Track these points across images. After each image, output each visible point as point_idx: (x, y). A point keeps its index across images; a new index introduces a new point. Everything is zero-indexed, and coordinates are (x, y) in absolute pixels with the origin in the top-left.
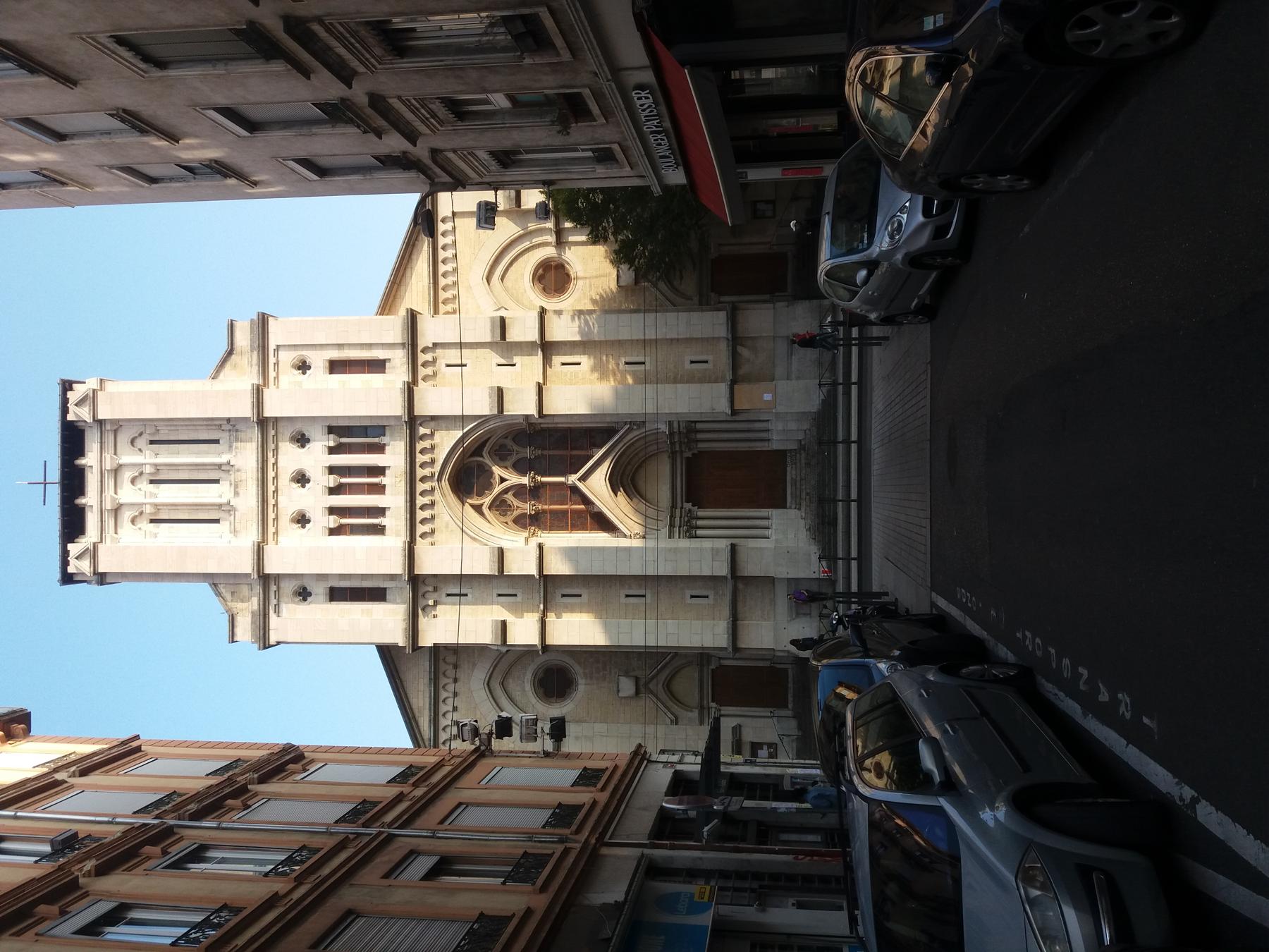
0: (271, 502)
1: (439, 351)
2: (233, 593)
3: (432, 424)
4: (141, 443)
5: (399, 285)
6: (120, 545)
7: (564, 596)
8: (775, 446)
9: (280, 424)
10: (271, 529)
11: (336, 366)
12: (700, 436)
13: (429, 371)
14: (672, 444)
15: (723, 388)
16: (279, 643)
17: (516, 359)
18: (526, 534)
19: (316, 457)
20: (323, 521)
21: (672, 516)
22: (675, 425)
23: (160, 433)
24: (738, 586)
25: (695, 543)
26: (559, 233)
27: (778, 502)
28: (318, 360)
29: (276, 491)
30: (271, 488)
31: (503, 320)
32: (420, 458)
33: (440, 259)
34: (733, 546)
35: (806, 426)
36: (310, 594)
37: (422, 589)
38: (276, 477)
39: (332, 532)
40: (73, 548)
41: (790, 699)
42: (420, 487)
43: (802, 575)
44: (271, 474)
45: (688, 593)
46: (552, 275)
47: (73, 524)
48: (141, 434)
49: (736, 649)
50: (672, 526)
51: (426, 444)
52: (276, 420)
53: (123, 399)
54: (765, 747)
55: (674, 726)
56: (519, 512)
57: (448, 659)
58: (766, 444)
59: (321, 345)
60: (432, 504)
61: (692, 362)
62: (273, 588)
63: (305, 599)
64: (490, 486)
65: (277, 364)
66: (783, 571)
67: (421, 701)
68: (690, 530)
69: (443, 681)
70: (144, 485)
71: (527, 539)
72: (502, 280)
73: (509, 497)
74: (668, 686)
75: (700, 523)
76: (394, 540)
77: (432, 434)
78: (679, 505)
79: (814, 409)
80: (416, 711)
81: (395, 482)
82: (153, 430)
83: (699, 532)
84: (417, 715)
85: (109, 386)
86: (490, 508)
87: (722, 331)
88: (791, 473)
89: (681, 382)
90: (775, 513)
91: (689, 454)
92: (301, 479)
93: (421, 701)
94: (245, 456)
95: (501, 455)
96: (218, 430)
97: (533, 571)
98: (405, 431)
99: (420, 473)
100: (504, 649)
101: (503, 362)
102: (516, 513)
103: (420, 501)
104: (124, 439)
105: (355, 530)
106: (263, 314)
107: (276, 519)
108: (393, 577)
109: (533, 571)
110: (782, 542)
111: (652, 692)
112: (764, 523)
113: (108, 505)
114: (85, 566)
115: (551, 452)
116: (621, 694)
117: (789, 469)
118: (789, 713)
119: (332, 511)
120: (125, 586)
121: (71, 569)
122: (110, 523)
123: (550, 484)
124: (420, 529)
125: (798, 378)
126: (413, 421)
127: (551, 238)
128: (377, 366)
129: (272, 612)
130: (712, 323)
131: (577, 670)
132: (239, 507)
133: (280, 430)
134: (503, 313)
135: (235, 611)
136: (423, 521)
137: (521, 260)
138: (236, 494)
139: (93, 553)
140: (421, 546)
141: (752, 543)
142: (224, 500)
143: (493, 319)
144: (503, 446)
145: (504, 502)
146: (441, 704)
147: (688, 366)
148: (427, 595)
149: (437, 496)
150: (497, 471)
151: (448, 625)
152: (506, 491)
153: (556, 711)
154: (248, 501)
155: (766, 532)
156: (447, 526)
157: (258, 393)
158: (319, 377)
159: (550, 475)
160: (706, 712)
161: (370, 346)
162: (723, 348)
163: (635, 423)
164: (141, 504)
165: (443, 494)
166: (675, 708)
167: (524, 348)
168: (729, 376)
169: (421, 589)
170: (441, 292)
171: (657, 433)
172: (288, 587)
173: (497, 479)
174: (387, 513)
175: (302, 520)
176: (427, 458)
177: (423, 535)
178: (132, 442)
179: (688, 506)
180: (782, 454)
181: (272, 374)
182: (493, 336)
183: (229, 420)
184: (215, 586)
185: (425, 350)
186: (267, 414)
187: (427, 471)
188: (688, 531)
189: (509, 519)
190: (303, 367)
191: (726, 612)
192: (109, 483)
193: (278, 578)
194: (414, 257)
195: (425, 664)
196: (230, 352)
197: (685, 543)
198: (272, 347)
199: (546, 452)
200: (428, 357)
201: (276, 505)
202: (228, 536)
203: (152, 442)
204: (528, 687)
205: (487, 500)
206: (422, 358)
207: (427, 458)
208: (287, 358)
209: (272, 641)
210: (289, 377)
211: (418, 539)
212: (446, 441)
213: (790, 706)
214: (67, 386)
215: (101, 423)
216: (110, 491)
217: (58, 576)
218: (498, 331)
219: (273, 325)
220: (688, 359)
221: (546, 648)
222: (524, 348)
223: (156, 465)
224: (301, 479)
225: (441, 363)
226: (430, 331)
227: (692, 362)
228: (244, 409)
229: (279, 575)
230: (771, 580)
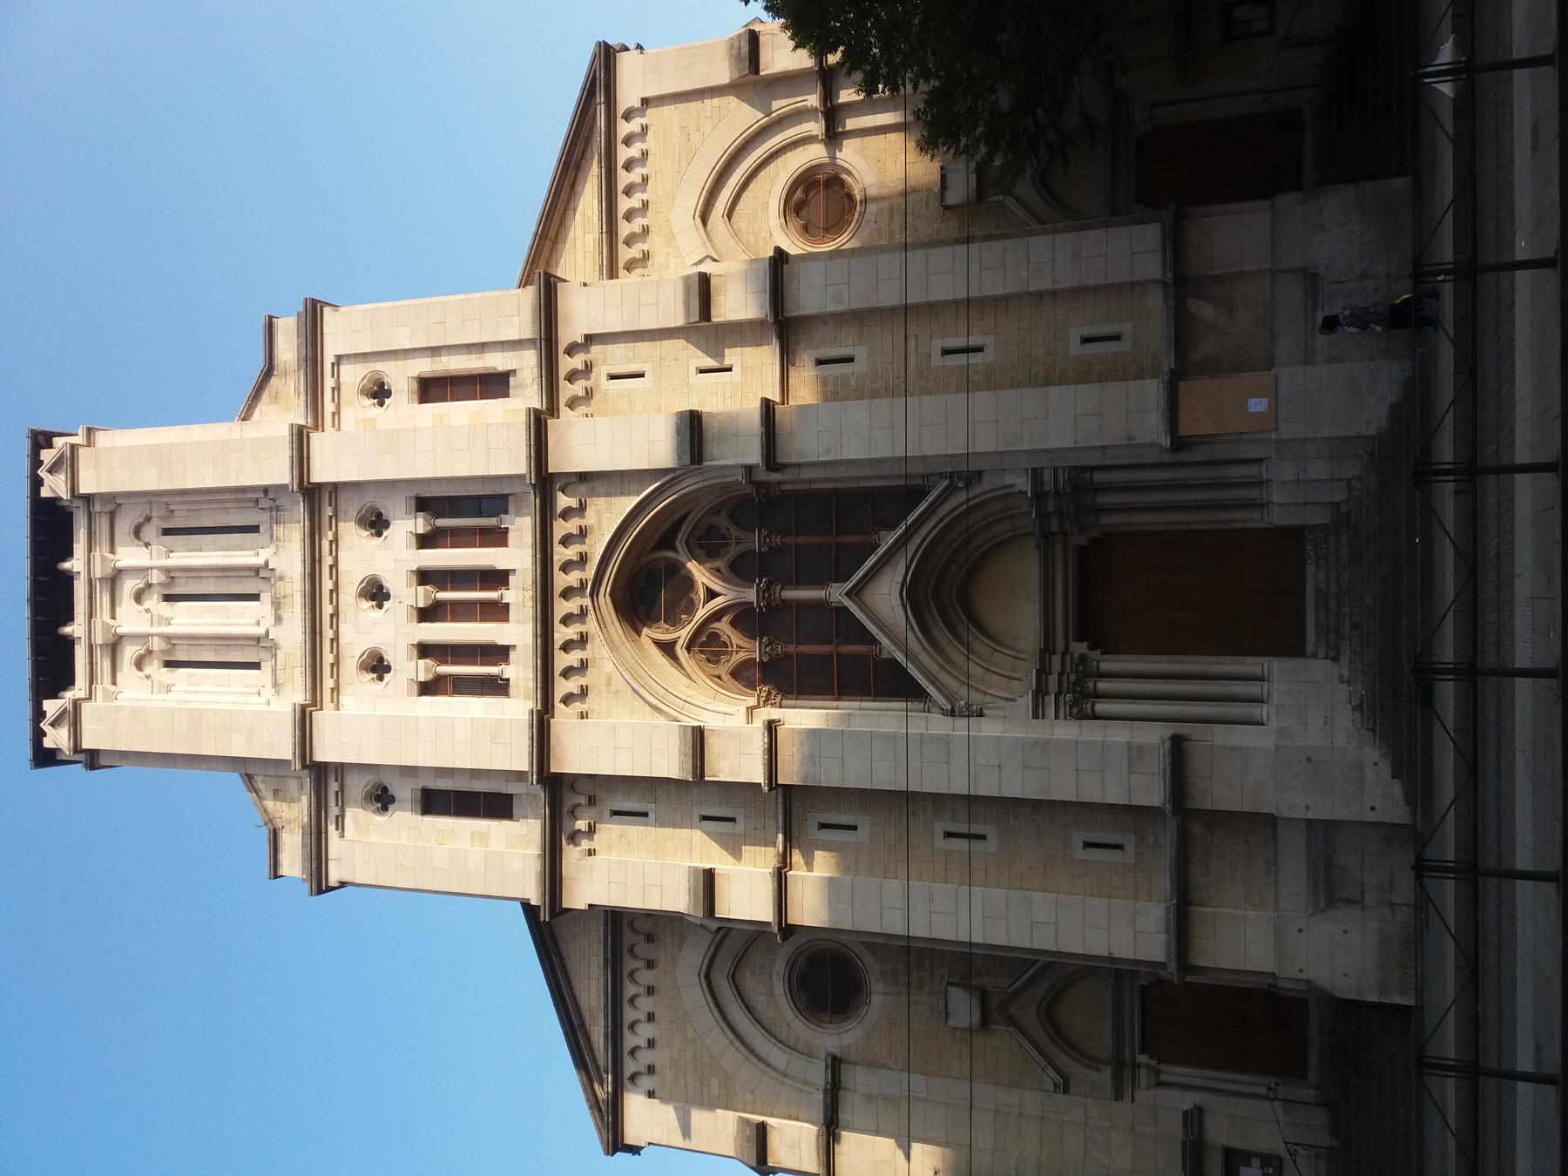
0: (328, 634)
1: (596, 349)
2: (276, 792)
3: (583, 488)
4: (149, 532)
5: (555, 242)
6: (124, 707)
7: (823, 826)
8: (1277, 518)
9: (343, 496)
10: (328, 683)
11: (431, 389)
12: (1103, 500)
13: (578, 388)
14: (1043, 517)
15: (1152, 391)
16: (343, 884)
17: (732, 356)
18: (752, 701)
19: (395, 554)
20: (408, 669)
21: (1043, 672)
22: (1048, 476)
23: (178, 514)
24: (1189, 832)
25: (1090, 732)
26: (832, 115)
27: (1284, 641)
28: (401, 376)
29: (335, 615)
30: (328, 609)
31: (704, 281)
32: (561, 554)
33: (621, 187)
34: (1178, 742)
35: (1351, 469)
36: (392, 800)
37: (570, 800)
38: (335, 590)
39: (426, 689)
40: (51, 707)
41: (1313, 1061)
42: (562, 607)
43: (1340, 814)
44: (327, 584)
45: (1078, 837)
46: (819, 199)
47: (52, 666)
48: (148, 519)
49: (1184, 965)
50: (1040, 692)
51: (571, 526)
52: (336, 487)
53: (116, 461)
54: (1256, 1162)
55: (1060, 1097)
56: (743, 656)
57: (623, 928)
58: (1256, 514)
59: (405, 351)
60: (583, 640)
61: (1086, 340)
62: (334, 786)
63: (385, 809)
64: (691, 609)
65: (337, 389)
66: (1297, 802)
67: (591, 996)
68: (1080, 702)
69: (629, 964)
70: (153, 602)
71: (750, 711)
72: (730, 216)
73: (723, 627)
74: (1049, 1014)
75: (1104, 686)
76: (518, 708)
77: (582, 508)
78: (1060, 647)
79: (1372, 431)
80: (586, 1014)
81: (519, 595)
82: (163, 513)
83: (1102, 707)
84: (587, 1022)
85: (102, 439)
86: (688, 649)
87: (1151, 267)
88: (1314, 578)
89: (1062, 380)
90: (1277, 667)
91: (1081, 540)
92: (376, 593)
93: (591, 996)
94: (285, 552)
95: (707, 549)
96: (238, 511)
97: (757, 775)
98: (532, 500)
99: (561, 580)
100: (714, 926)
101: (711, 363)
102: (737, 658)
103: (562, 634)
104: (124, 525)
105: (462, 686)
106: (314, 302)
107: (336, 664)
108: (520, 776)
109: (757, 775)
110: (1292, 736)
111: (1013, 1022)
112: (1253, 689)
113: (99, 639)
114: (57, 738)
115: (803, 540)
116: (952, 1022)
117: (1310, 569)
118: (1306, 1093)
119: (425, 650)
120: (126, 772)
121: (48, 743)
122: (104, 665)
123: (800, 605)
124: (562, 687)
125: (1331, 360)
126: (545, 482)
127: (816, 127)
128: (494, 384)
129: (332, 827)
130: (1131, 251)
131: (871, 966)
132: (282, 642)
133: (342, 505)
134: (707, 268)
135: (279, 823)
136: (567, 672)
137: (763, 174)
138: (278, 619)
139: (73, 717)
140: (564, 718)
141: (1224, 736)
142: (261, 631)
143: (687, 279)
144: (712, 530)
145: (714, 636)
146: (627, 1008)
147: (1075, 348)
148: (579, 811)
149: (591, 625)
150: (701, 575)
151: (634, 869)
152: (717, 616)
153: (830, 1039)
154: (291, 635)
155: (1255, 711)
156: (609, 683)
157: (301, 438)
158: (403, 407)
159: (798, 584)
160: (1127, 1073)
161: (482, 347)
162: (1155, 301)
163: (964, 474)
164: (146, 636)
165: (601, 623)
166: (1063, 1059)
167: (739, 333)
168: (1168, 363)
169: (567, 802)
170: (622, 248)
171: (1007, 495)
172: (357, 786)
173: (701, 592)
174: (513, 655)
175: (377, 666)
176: (571, 553)
177: (568, 699)
178: (137, 532)
179: (1080, 648)
180: (1296, 534)
181: (329, 407)
182: (688, 315)
183: (266, 490)
184: (249, 778)
185: (571, 350)
186: (317, 477)
187: (573, 578)
188: (1075, 703)
189: (723, 669)
190: (379, 392)
191: (1164, 883)
192: (103, 599)
193: (341, 769)
194: (578, 189)
195: (597, 931)
196: (268, 372)
197: (1067, 731)
198: (329, 359)
199: (790, 540)
200: (576, 362)
201: (335, 640)
202: (268, 691)
203: (167, 532)
204: (779, 987)
205: (684, 633)
206: (567, 364)
207: (571, 553)
208: (353, 375)
209: (333, 879)
210: (358, 411)
211: (559, 706)
212: (606, 516)
213: (1313, 1078)
214: (41, 440)
215: (88, 499)
216: (103, 615)
217: (28, 753)
218: (695, 303)
219: (332, 322)
220: (1075, 333)
221: (788, 930)
222: (739, 333)
223: (167, 571)
224: (376, 593)
225: (600, 372)
226: (582, 311)
227: (1086, 340)
228: (278, 472)
229: (342, 764)
230: (1269, 823)
